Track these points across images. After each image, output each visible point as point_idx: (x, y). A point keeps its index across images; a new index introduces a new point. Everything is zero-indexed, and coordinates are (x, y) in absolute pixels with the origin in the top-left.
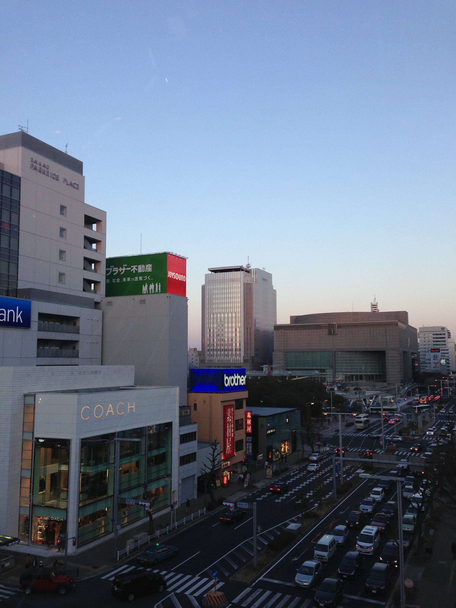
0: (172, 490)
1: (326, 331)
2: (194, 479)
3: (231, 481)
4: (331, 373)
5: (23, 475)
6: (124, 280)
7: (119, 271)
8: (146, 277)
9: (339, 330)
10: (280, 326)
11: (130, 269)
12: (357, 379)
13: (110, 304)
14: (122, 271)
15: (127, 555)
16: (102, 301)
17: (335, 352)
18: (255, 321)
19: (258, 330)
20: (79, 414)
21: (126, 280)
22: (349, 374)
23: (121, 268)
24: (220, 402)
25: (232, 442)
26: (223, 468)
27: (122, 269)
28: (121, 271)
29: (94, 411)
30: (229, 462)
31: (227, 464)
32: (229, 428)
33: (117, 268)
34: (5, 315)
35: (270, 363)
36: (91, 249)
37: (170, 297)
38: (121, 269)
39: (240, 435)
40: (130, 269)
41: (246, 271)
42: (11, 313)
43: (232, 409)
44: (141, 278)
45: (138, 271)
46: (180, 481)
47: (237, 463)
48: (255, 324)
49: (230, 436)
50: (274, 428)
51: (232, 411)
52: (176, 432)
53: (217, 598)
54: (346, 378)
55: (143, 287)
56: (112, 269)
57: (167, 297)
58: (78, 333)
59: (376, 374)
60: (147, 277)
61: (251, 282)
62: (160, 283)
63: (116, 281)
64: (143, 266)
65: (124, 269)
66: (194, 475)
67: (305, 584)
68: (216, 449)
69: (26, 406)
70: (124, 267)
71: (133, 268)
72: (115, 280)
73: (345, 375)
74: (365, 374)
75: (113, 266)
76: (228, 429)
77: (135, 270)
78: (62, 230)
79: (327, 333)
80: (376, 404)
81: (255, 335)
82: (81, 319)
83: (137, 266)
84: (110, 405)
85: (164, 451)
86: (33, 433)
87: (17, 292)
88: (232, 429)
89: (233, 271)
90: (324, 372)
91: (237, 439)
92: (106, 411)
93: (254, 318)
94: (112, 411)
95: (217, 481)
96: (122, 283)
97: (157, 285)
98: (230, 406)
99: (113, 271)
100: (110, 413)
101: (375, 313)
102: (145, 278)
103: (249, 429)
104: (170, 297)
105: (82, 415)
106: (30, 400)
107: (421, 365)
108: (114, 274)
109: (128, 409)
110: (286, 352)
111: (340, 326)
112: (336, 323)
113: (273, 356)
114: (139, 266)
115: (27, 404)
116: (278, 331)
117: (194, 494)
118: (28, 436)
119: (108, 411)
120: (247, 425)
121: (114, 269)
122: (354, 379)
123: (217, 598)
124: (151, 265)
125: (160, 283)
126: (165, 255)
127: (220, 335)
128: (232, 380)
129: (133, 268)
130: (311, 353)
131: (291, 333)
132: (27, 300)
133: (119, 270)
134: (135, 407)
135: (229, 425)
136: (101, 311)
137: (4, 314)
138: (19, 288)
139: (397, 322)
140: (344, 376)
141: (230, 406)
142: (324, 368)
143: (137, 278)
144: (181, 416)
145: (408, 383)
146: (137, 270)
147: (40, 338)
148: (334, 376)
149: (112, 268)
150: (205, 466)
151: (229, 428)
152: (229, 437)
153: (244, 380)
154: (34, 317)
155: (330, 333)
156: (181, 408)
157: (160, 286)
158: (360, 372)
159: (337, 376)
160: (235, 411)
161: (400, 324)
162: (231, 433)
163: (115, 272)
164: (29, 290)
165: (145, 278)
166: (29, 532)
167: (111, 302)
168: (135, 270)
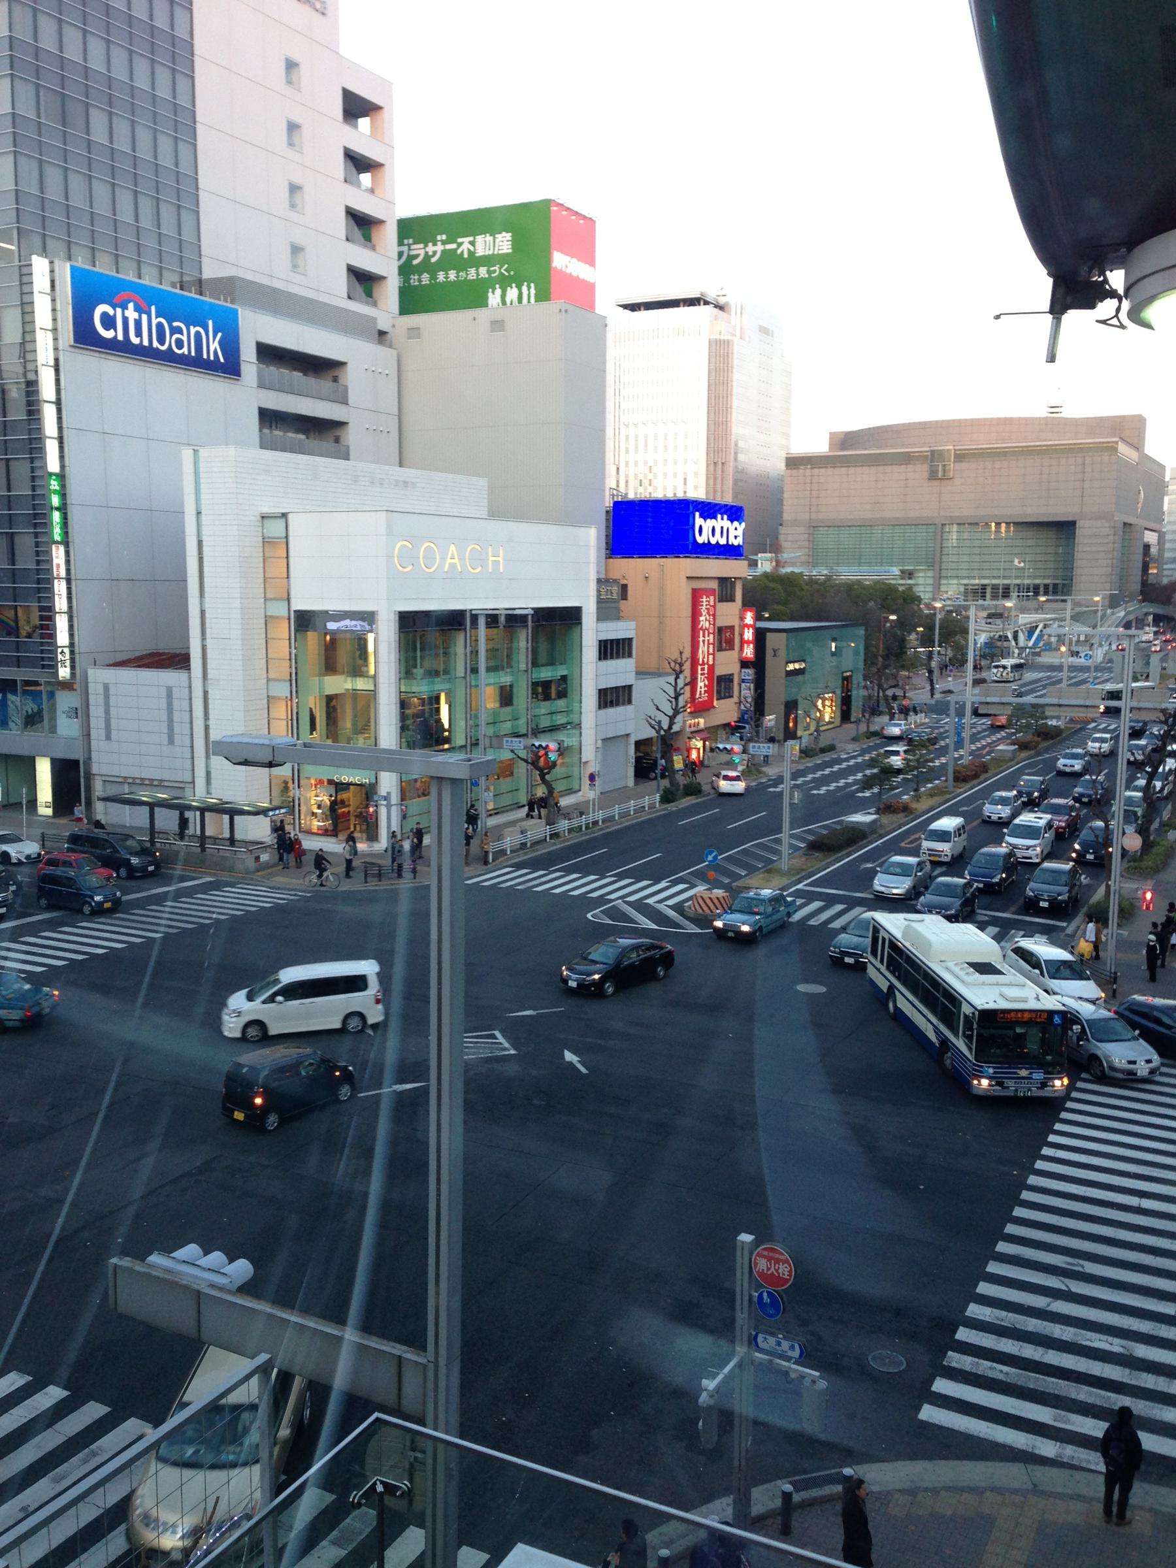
0: (583, 760)
1: (922, 470)
2: (627, 744)
3: (706, 763)
4: (930, 581)
5: (271, 694)
6: (441, 277)
7: (426, 253)
8: (496, 268)
9: (958, 466)
10: (803, 458)
11: (454, 246)
12: (995, 597)
13: (414, 332)
14: (435, 253)
15: (506, 854)
16: (394, 326)
17: (943, 525)
18: (736, 445)
19: (742, 471)
20: (390, 556)
21: (447, 278)
22: (977, 582)
23: (430, 244)
24: (685, 579)
25: (710, 676)
26: (688, 729)
27: (435, 248)
28: (431, 253)
29: (419, 554)
30: (702, 721)
31: (698, 723)
32: (704, 641)
33: (421, 246)
34: (185, 338)
35: (775, 548)
36: (358, 184)
37: (566, 311)
38: (430, 249)
39: (728, 663)
40: (454, 246)
41: (716, 307)
42: (198, 334)
43: (712, 598)
44: (483, 271)
45: (474, 253)
46: (600, 742)
47: (718, 726)
48: (736, 453)
49: (706, 660)
50: (804, 661)
51: (712, 603)
52: (591, 632)
53: (716, 901)
54: (966, 592)
55: (490, 295)
56: (410, 249)
57: (560, 311)
58: (345, 402)
59: (1046, 582)
60: (500, 268)
61: (730, 338)
62: (532, 285)
63: (420, 281)
64: (489, 238)
65: (439, 248)
66: (628, 735)
67: (895, 891)
68: (681, 672)
69: (266, 542)
70: (439, 243)
71: (462, 243)
72: (416, 277)
73: (965, 585)
74: (1018, 582)
75: (411, 241)
76: (701, 643)
77: (469, 250)
78: (293, 127)
79: (926, 475)
80: (1044, 645)
81: (736, 482)
82: (349, 366)
83: (471, 239)
84: (452, 547)
85: (565, 673)
86: (289, 600)
87: (200, 285)
88: (711, 646)
89: (682, 304)
90: (910, 578)
91: (720, 671)
92: (443, 559)
93: (733, 437)
94: (456, 561)
95: (675, 758)
96: (434, 286)
97: (524, 289)
98: (710, 592)
99: (412, 253)
100: (453, 566)
101: (1054, 423)
102: (495, 271)
103: (749, 652)
104: (566, 311)
105: (396, 559)
106: (275, 529)
107: (1165, 567)
108: (415, 262)
109: (490, 563)
110: (813, 527)
111: (961, 457)
112: (951, 447)
113: (782, 537)
114: (480, 239)
115: (269, 538)
116: (795, 472)
117: (626, 777)
118: (279, 610)
119: (449, 561)
120: (743, 642)
121: (413, 247)
122: (988, 596)
123: (716, 901)
124: (508, 236)
125: (532, 285)
126: (547, 203)
127: (646, 482)
128: (713, 529)
129: (462, 243)
130: (880, 528)
131: (831, 478)
132: (229, 305)
133: (428, 249)
134: (504, 560)
135: (704, 636)
136: (393, 353)
137: (182, 334)
138: (205, 276)
139: (1117, 443)
140: (962, 589)
141: (710, 592)
142: (912, 568)
143: (473, 271)
144: (600, 602)
145: (1127, 602)
146: (472, 248)
147: (263, 406)
148: (937, 587)
149: (409, 245)
150: (658, 709)
151: (704, 641)
152: (703, 664)
153: (740, 532)
154: (248, 353)
155: (933, 476)
156: (599, 581)
157: (533, 291)
158: (1004, 577)
159: (943, 588)
160: (720, 606)
161: (1123, 448)
162: (709, 654)
163: (417, 256)
164: (232, 280)
165: (495, 271)
166: (294, 811)
167: (418, 328)
168: (469, 250)
